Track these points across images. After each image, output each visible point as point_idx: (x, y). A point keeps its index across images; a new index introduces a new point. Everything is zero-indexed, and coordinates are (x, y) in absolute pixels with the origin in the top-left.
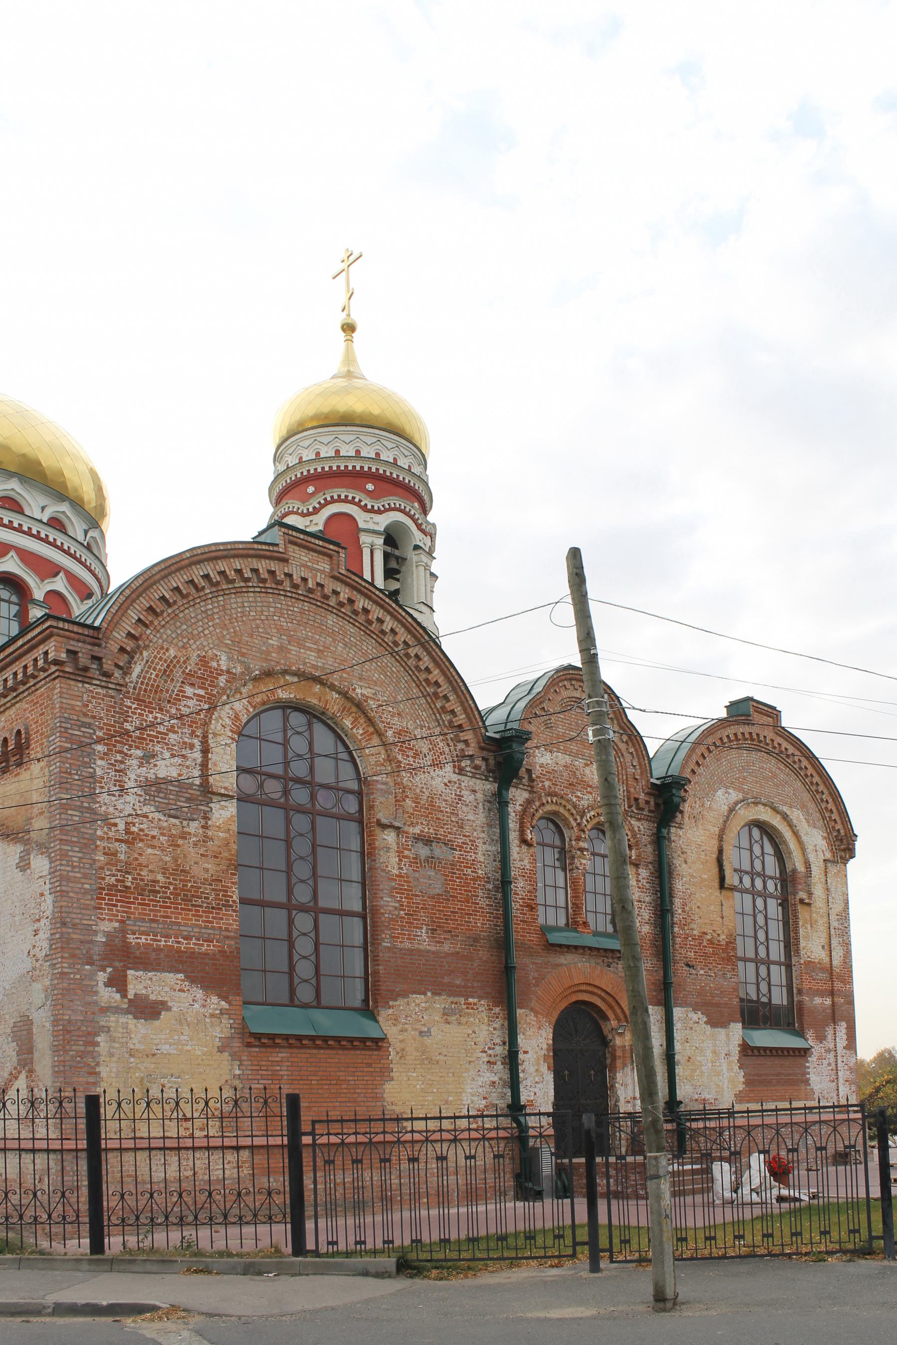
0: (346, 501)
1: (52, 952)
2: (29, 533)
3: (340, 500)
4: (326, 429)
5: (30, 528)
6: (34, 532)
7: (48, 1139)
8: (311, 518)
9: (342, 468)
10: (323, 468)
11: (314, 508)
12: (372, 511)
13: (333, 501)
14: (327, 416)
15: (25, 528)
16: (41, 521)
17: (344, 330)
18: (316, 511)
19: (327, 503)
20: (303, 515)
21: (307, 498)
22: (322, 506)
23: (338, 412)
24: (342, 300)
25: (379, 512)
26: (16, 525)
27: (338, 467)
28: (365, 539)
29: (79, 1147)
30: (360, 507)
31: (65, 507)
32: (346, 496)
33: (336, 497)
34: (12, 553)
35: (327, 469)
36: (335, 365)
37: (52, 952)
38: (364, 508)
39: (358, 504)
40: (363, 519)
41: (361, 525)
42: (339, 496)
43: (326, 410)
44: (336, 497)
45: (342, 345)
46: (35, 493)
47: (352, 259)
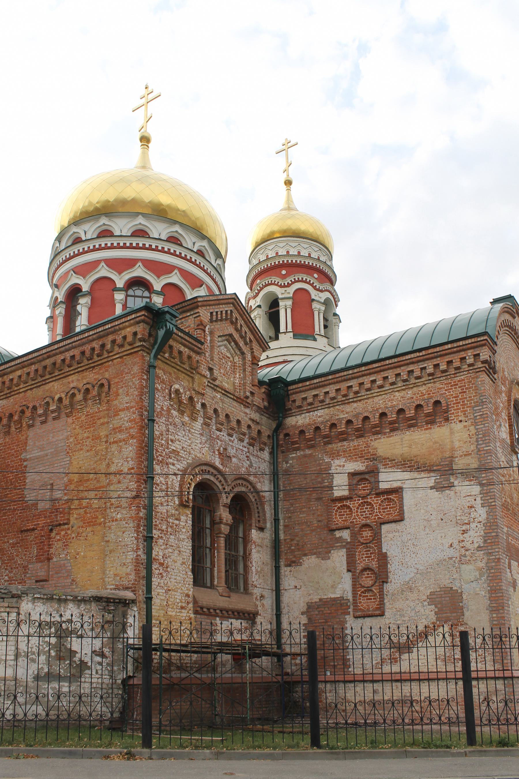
0: (305, 282)
1: (485, 545)
2: (185, 258)
3: (302, 281)
4: (292, 239)
5: (186, 255)
6: (188, 258)
7: (486, 671)
8: (286, 289)
9: (290, 262)
10: (292, 261)
11: (288, 283)
12: (318, 290)
13: (299, 281)
14: (285, 231)
15: (178, 253)
16: (192, 251)
17: (285, 183)
18: (289, 285)
19: (296, 281)
20: (281, 286)
21: (284, 277)
22: (293, 283)
23: (291, 229)
24: (284, 166)
25: (322, 291)
26: (154, 247)
27: (288, 261)
28: (315, 305)
29: (457, 676)
30: (313, 286)
31: (205, 243)
32: (306, 279)
33: (300, 279)
34: (176, 271)
35: (294, 262)
36: (281, 203)
37: (485, 545)
38: (315, 288)
39: (312, 285)
40: (314, 294)
41: (280, 296)
42: (302, 278)
43: (285, 227)
44: (300, 279)
45: (285, 193)
46: (153, 222)
47: (288, 146)
